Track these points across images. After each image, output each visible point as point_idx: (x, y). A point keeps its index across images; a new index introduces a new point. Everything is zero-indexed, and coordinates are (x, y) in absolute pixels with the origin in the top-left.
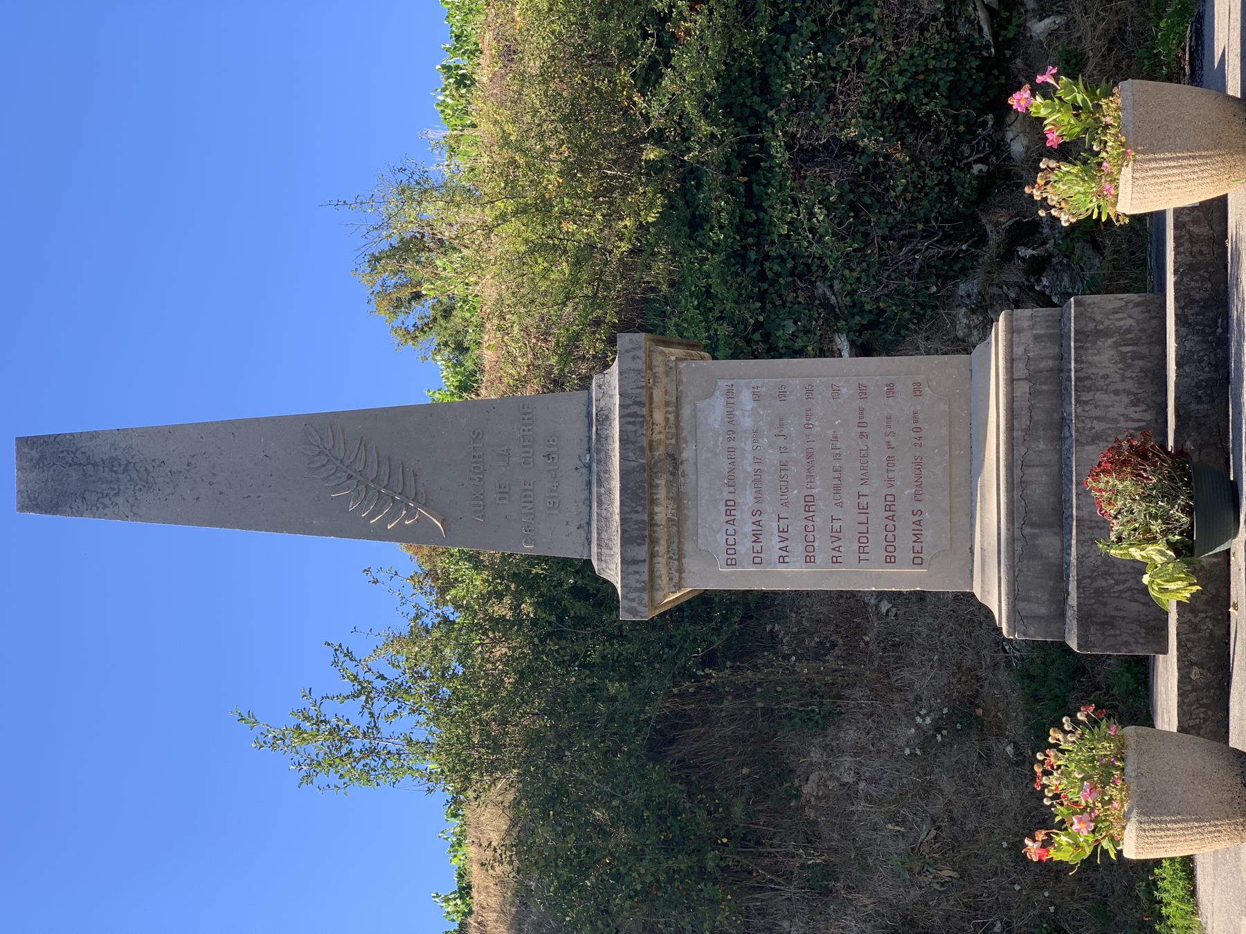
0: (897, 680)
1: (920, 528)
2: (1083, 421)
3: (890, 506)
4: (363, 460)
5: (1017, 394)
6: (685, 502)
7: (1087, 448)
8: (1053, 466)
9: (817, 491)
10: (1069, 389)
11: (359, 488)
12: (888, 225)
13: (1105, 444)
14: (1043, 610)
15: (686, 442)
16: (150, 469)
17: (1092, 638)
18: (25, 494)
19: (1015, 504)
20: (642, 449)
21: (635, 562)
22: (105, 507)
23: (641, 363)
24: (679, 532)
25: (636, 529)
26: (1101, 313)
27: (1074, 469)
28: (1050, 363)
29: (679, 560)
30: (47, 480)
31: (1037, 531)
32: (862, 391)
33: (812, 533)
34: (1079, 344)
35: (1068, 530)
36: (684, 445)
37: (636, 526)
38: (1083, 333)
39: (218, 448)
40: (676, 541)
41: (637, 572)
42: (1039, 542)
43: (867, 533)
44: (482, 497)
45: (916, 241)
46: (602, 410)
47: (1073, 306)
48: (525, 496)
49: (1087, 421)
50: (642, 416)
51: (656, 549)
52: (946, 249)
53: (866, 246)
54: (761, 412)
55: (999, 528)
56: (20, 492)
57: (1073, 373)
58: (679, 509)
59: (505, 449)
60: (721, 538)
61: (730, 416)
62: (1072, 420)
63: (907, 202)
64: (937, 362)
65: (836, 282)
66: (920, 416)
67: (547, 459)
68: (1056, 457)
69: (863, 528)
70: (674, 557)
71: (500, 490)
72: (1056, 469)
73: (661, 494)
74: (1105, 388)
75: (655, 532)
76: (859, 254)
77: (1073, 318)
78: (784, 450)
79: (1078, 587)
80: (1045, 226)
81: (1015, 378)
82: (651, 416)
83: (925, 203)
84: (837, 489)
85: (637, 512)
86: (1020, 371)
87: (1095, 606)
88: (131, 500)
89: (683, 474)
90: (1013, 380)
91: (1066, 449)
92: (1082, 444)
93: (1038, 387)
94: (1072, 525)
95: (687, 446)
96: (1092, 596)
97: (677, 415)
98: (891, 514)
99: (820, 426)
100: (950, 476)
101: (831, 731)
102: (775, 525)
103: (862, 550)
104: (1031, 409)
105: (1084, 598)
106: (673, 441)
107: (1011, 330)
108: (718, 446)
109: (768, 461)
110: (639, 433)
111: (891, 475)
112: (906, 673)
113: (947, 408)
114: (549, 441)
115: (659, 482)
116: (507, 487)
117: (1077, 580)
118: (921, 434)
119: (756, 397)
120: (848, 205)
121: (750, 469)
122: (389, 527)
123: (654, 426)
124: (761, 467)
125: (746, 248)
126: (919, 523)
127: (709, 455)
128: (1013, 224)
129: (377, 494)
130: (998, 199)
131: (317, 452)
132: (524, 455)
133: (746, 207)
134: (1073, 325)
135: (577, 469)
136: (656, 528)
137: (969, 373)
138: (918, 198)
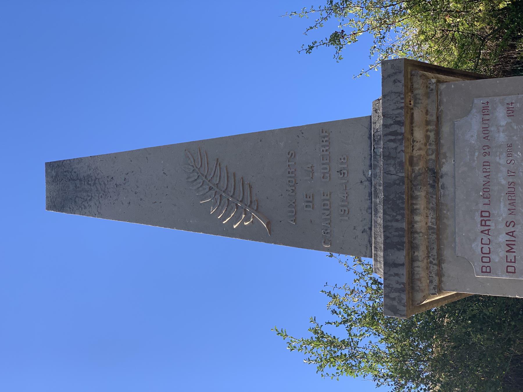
4: (219, 176)
6: (445, 212)
11: (216, 197)
15: (445, 157)
16: (106, 182)
18: (49, 199)
21: (396, 265)
22: (85, 208)
24: (438, 239)
29: (439, 264)
30: (59, 189)
36: (444, 160)
37: (397, 233)
39: (140, 168)
41: (397, 275)
44: (294, 205)
46: (377, 131)
48: (324, 205)
50: (402, 134)
51: (416, 254)
54: (515, 127)
56: (47, 197)
58: (439, 218)
59: (310, 166)
60: (477, 246)
61: (486, 132)
67: (339, 173)
70: (434, 262)
71: (307, 199)
73: (421, 204)
75: (415, 239)
82: (412, 134)
85: (397, 221)
88: (97, 203)
89: (443, 187)
95: (447, 161)
97: (438, 133)
106: (433, 157)
108: (474, 161)
110: (399, 150)
114: (341, 159)
116: (311, 197)
119: (511, 112)
121: (504, 182)
122: (235, 227)
124: (515, 180)
129: (227, 201)
131: (192, 170)
132: (323, 171)
136: (416, 235)
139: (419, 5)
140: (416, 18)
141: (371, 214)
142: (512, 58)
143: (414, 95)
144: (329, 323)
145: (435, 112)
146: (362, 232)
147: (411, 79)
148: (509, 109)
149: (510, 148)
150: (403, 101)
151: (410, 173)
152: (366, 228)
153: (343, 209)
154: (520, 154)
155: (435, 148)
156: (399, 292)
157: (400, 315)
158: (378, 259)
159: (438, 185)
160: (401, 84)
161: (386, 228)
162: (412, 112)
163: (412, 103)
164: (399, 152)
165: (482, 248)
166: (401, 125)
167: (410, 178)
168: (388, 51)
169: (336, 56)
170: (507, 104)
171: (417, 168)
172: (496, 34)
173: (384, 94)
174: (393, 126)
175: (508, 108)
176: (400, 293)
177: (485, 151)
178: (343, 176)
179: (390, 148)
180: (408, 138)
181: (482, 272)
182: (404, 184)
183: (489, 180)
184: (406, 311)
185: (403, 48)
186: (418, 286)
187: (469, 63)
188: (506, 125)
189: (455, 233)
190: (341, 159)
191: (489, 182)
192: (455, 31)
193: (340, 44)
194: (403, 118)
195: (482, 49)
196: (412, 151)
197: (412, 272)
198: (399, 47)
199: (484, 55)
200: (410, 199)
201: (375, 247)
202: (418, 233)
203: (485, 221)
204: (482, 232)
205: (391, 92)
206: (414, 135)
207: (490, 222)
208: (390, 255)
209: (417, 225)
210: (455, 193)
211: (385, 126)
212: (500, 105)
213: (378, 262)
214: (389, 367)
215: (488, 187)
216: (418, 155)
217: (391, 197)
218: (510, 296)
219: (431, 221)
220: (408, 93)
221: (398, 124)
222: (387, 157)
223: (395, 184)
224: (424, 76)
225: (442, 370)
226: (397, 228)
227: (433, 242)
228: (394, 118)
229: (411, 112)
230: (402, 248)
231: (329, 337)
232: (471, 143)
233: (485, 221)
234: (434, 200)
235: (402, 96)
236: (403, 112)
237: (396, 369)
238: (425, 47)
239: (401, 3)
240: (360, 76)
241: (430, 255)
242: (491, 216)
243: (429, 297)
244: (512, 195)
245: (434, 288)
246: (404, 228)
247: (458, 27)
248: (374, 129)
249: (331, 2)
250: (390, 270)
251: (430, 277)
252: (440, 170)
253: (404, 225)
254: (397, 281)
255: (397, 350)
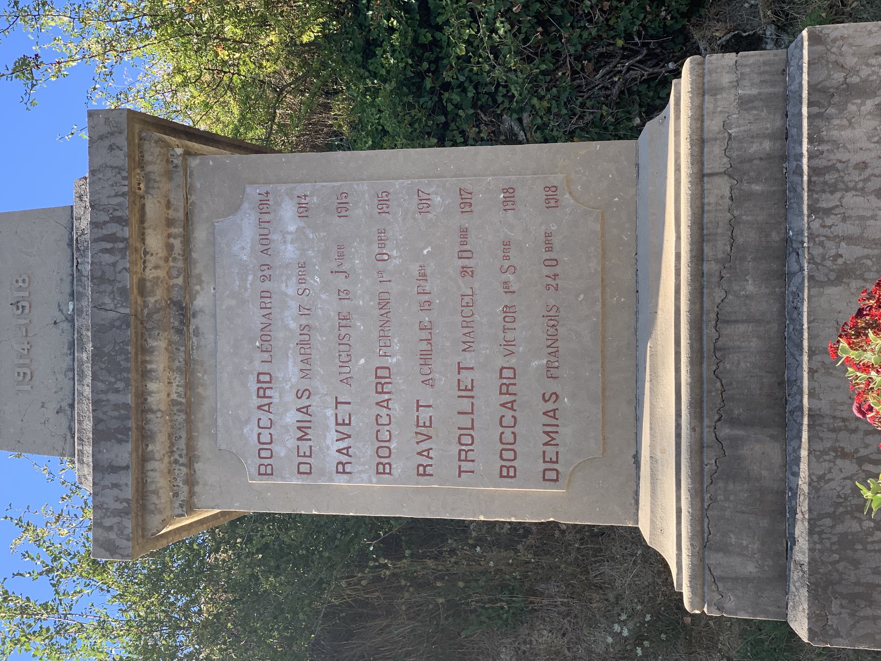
0: (596, 576)
1: (554, 422)
2: (822, 244)
3: (508, 386)
5: (710, 199)
6: (200, 375)
7: (830, 290)
8: (768, 322)
9: (394, 360)
10: (799, 189)
12: (581, 41)
13: (860, 283)
14: (751, 568)
15: (200, 282)
17: (833, 621)
19: (705, 386)
20: (124, 292)
21: (114, 469)
23: (122, 157)
24: (189, 421)
25: (115, 418)
26: (854, 54)
27: (805, 326)
28: (767, 145)
29: (190, 464)
31: (741, 433)
32: (466, 201)
33: (387, 428)
34: (816, 110)
35: (795, 432)
36: (198, 288)
37: (116, 413)
38: (824, 91)
40: (184, 434)
41: (115, 486)
42: (745, 451)
43: (472, 428)
45: (615, 61)
46: (83, 234)
47: (806, 44)
49: (828, 244)
51: (150, 448)
52: (651, 70)
53: (557, 69)
54: (311, 236)
55: (678, 426)
57: (805, 161)
58: (189, 386)
60: (251, 431)
61: (264, 242)
62: (802, 242)
63: (605, 12)
64: (583, 152)
65: (525, 116)
66: (556, 241)
67: (14, 307)
68: (775, 308)
69: (466, 421)
70: (181, 461)
72: (775, 327)
73: (159, 362)
74: (860, 185)
75: (148, 422)
76: (548, 78)
77: (805, 66)
78: (343, 295)
79: (811, 532)
80: (769, 41)
81: (706, 171)
82: (143, 241)
83: (626, 13)
84: (426, 357)
85: (117, 391)
86: (716, 160)
87: (841, 566)
89: (197, 332)
90: (703, 176)
91: (793, 293)
92: (821, 284)
93: (745, 186)
94: (802, 424)
95: (202, 289)
96: (835, 547)
97: (187, 241)
98: (508, 398)
99: (401, 257)
100: (604, 338)
101: (523, 630)
102: (330, 413)
103: (463, 456)
104: (733, 224)
105: (821, 551)
106: (180, 281)
107: (701, 91)
108: (246, 289)
109: (320, 311)
110: (120, 267)
111: (509, 336)
112: (605, 568)
113: (598, 227)
114: (17, 281)
115: (155, 344)
117: (809, 520)
118: (558, 270)
119: (304, 211)
120: (535, 17)
121: (293, 325)
123: (148, 257)
124: (310, 322)
125: (421, 76)
126: (552, 414)
127: (233, 302)
128: (731, 38)
130: (713, 11)
133: (420, 26)
134: (805, 76)
135: (55, 323)
136: (150, 416)
137: (634, 170)
138: (617, 7)
139: (172, 24)
140: (167, 44)
141: (74, 379)
142: (326, 126)
143: (145, 174)
144: (19, 574)
145: (181, 204)
146: (57, 413)
147: (140, 146)
148: (301, 205)
149: (302, 269)
150: (126, 183)
151: (139, 309)
152: (65, 404)
153: (21, 371)
154: (318, 280)
155: (183, 266)
156: (118, 516)
157: (122, 555)
158: (85, 460)
159: (188, 330)
160: (123, 152)
161: (97, 404)
162: (142, 202)
163: (142, 186)
164: (120, 272)
165: (259, 434)
166: (123, 223)
167: (140, 317)
168: (119, 96)
169: (26, 98)
170: (298, 197)
171: (152, 300)
172: (299, 85)
173: (92, 168)
174: (109, 225)
175: (299, 204)
176: (121, 517)
177: (264, 273)
178: (22, 312)
179: (103, 263)
180: (136, 248)
181: (260, 474)
182: (128, 326)
183: (270, 322)
184: (131, 549)
185: (147, 95)
186: (154, 503)
187: (257, 129)
188: (296, 231)
189: (216, 410)
190: (17, 281)
191: (270, 324)
192: (233, 74)
193: (33, 78)
194: (127, 212)
195: (278, 108)
196: (144, 271)
197: (142, 479)
198: (138, 91)
199: (283, 118)
200: (139, 353)
201: (80, 439)
202: (153, 412)
203: (265, 389)
204: (259, 408)
205: (104, 165)
206: (147, 242)
207: (273, 391)
208: (105, 451)
209: (153, 399)
210: (216, 343)
211: (94, 224)
212: (287, 198)
213: (85, 465)
214: (125, 644)
215: (269, 333)
216: (154, 278)
217: (106, 350)
218: (303, 512)
219: (176, 390)
220: (135, 169)
221: (117, 222)
222: (99, 279)
223: (113, 326)
224: (163, 141)
225: (213, 641)
226: (116, 405)
227: (179, 427)
228: (111, 212)
229: (140, 202)
230: (125, 438)
231: (17, 598)
232: (241, 260)
233: (265, 389)
234: (182, 354)
235: (125, 174)
236: (125, 201)
237: (137, 647)
238: (184, 96)
239: (140, 18)
240: (70, 136)
241: (175, 449)
242: (273, 381)
243: (172, 521)
244: (305, 346)
245: (181, 506)
246: (128, 404)
247: (238, 67)
248: (77, 229)
249: (16, 3)
250: (103, 478)
251: (174, 486)
252: (192, 304)
253: (130, 399)
254: (117, 497)
255: (139, 614)
